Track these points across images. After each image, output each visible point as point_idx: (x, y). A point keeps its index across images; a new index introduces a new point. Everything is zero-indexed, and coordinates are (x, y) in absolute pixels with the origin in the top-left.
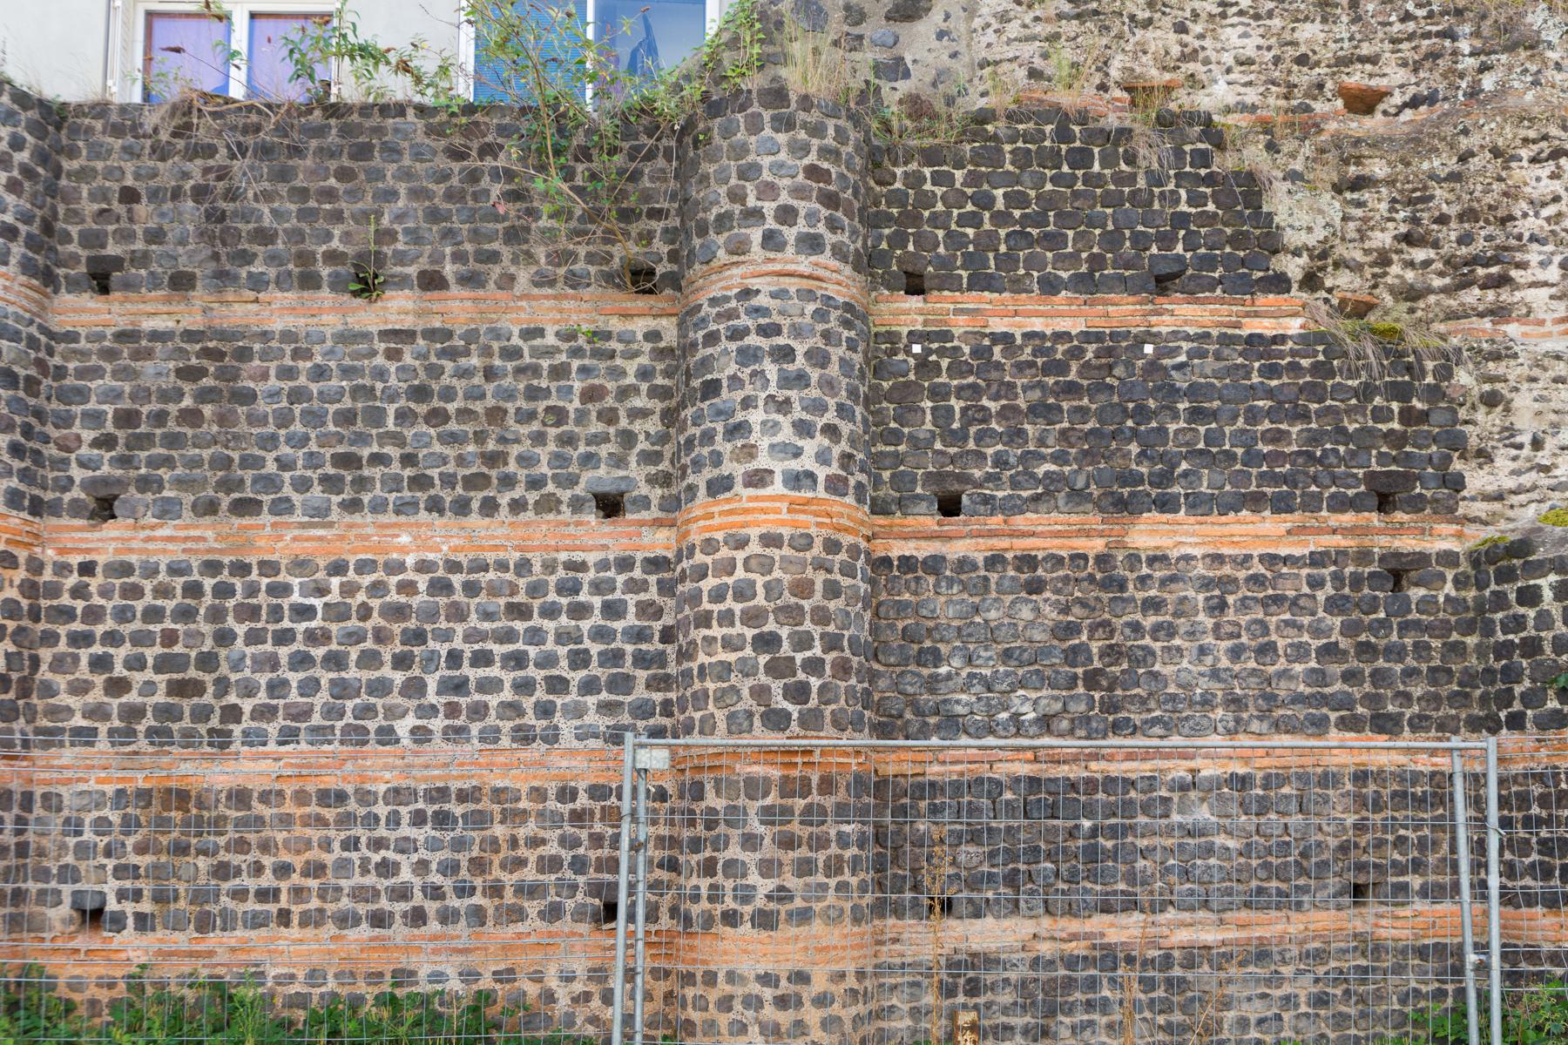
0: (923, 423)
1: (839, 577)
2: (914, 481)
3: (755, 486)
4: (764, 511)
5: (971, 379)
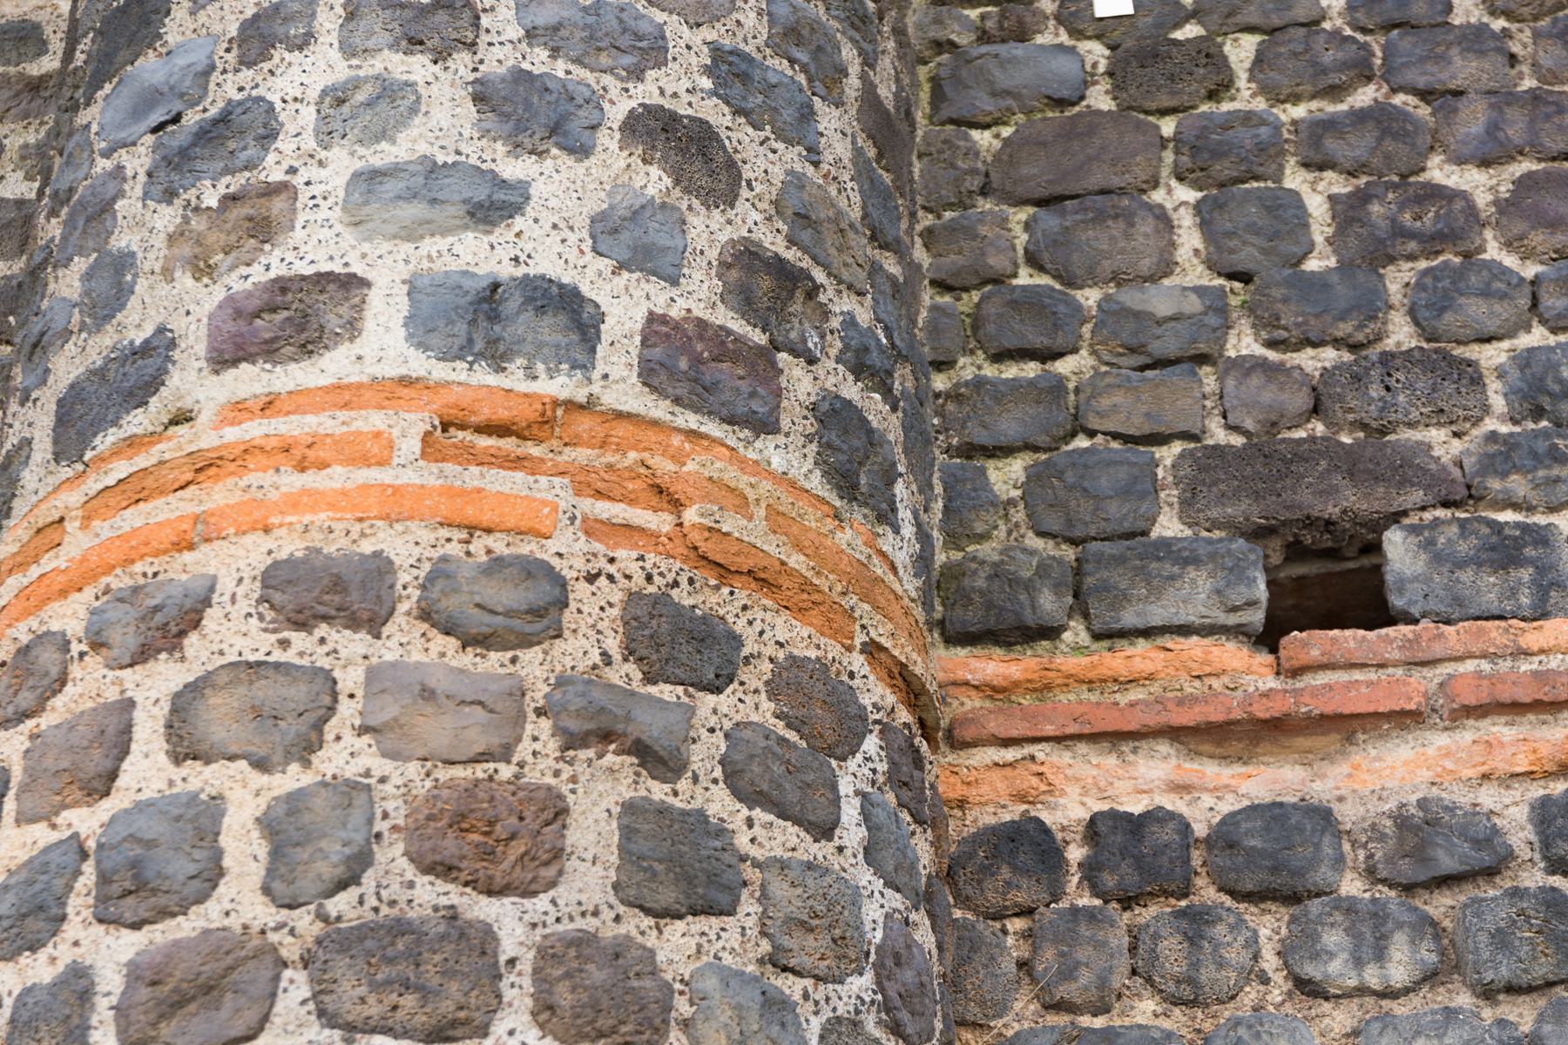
0: (1167, 267)
1: (720, 803)
2: (1144, 487)
3: (269, 351)
4: (302, 455)
5: (1365, 96)
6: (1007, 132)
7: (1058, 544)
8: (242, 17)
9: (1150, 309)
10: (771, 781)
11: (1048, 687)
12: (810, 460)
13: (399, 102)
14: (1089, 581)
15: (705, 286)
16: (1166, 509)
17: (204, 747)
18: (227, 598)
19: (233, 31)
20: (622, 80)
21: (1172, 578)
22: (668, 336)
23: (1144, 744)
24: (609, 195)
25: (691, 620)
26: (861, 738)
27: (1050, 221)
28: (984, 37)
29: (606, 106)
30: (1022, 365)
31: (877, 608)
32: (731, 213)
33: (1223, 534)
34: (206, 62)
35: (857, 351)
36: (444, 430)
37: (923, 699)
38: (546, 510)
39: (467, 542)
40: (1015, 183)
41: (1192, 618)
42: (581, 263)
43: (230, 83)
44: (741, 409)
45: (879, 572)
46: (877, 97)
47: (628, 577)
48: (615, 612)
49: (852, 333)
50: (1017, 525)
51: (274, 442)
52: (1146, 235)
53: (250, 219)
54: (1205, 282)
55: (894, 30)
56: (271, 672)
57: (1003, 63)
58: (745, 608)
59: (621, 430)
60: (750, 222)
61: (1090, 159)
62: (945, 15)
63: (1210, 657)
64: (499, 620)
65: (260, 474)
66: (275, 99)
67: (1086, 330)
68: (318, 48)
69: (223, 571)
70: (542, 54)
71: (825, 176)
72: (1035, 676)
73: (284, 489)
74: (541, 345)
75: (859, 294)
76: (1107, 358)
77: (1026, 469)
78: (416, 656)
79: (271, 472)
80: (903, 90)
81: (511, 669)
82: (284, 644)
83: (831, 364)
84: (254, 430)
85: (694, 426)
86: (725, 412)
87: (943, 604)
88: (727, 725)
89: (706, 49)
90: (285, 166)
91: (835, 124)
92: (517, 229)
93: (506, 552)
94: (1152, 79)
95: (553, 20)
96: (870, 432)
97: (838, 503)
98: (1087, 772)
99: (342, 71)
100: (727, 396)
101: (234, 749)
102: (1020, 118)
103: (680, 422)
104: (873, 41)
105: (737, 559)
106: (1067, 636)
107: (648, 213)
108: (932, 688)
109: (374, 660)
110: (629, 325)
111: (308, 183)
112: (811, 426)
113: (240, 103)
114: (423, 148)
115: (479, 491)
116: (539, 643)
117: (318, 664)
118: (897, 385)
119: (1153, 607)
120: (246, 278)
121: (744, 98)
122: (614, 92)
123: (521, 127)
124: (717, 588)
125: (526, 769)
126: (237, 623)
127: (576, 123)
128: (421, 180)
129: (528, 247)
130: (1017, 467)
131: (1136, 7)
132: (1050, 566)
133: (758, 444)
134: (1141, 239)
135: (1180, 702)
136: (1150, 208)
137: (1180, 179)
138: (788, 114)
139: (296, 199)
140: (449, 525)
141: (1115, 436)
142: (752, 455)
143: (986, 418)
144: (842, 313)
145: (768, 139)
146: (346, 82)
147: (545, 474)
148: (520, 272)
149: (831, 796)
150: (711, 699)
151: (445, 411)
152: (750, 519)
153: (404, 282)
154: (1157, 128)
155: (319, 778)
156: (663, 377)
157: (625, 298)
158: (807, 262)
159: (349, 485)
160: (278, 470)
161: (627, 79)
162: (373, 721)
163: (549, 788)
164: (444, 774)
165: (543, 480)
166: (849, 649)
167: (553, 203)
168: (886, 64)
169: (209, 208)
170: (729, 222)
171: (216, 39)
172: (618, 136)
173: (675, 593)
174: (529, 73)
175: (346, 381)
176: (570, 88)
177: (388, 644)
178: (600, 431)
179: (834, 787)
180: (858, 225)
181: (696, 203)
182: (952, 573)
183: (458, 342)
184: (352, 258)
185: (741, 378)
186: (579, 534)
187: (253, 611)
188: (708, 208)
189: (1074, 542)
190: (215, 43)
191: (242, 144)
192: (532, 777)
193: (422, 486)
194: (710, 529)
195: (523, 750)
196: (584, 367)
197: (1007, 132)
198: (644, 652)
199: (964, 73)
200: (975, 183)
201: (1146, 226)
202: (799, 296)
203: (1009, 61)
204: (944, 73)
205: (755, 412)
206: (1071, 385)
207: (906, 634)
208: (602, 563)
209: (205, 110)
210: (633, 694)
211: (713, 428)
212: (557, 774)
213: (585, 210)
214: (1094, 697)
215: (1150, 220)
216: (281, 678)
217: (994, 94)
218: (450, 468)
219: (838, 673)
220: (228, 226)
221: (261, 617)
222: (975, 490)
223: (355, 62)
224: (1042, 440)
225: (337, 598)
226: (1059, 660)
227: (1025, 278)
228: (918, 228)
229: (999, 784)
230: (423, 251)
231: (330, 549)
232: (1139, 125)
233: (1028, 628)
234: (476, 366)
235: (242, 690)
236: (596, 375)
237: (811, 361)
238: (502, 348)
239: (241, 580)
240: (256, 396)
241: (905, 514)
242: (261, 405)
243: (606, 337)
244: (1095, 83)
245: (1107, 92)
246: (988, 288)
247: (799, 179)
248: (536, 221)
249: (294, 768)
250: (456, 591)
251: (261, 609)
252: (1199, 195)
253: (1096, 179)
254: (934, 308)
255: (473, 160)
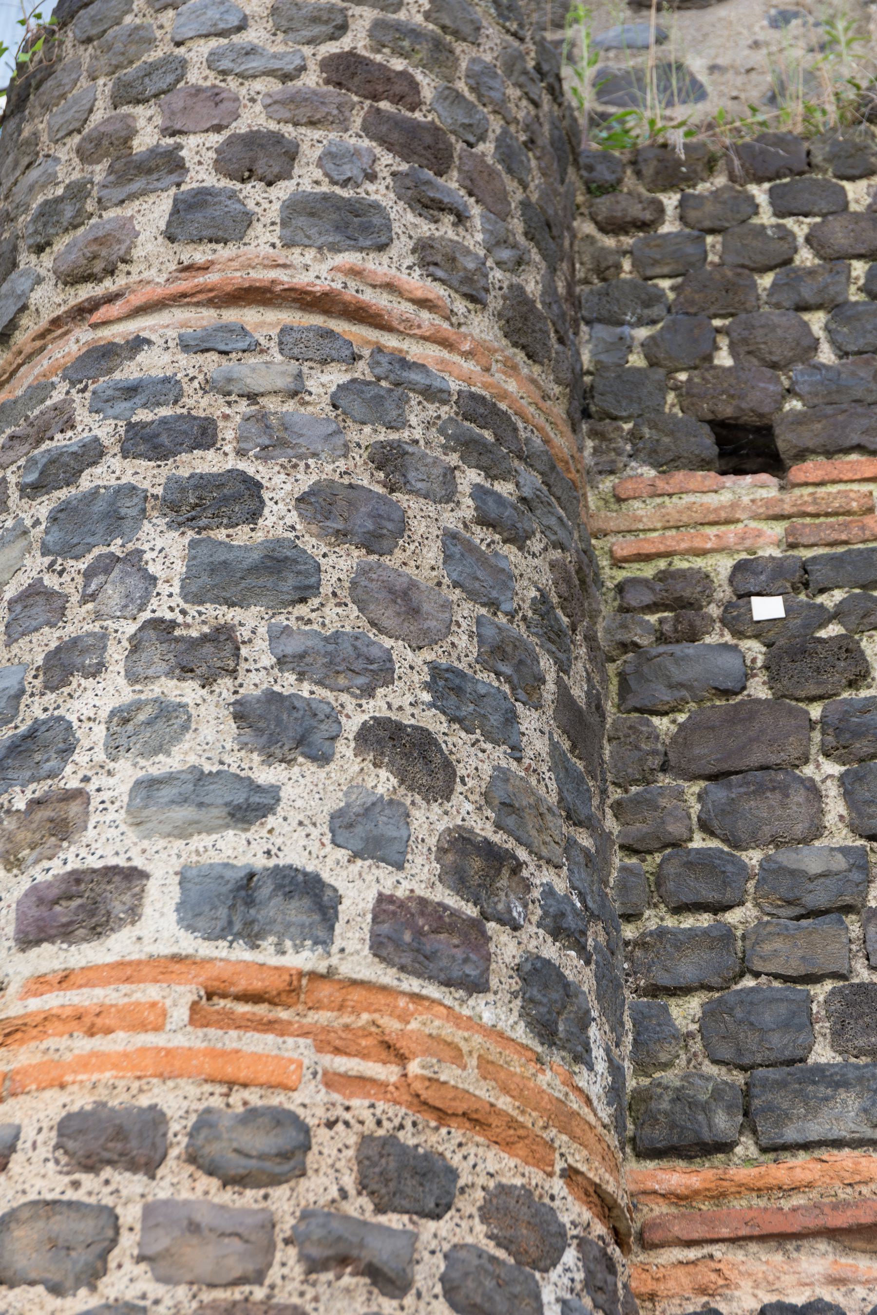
0: (817, 830)
6: (682, 718)
7: (730, 1070)
8: (47, 649)
9: (803, 868)
10: (483, 1295)
11: (723, 1195)
12: (516, 1013)
13: (173, 721)
14: (756, 1103)
15: (426, 869)
16: (820, 1039)
17: (9, 1274)
18: (29, 1144)
19: (40, 660)
20: (356, 697)
21: (826, 1099)
22: (394, 913)
23: (805, 1243)
24: (346, 794)
25: (415, 1157)
26: (561, 1252)
27: (719, 793)
28: (662, 638)
29: (343, 720)
30: (698, 916)
31: (573, 1138)
32: (447, 806)
33: (869, 1060)
34: (17, 687)
35: (555, 917)
36: (209, 998)
37: (616, 1212)
38: (293, 1067)
39: (227, 1095)
40: (689, 761)
41: (844, 1133)
42: (322, 853)
43: (36, 705)
44: (456, 973)
45: (575, 1106)
46: (571, 697)
47: (362, 1123)
48: (351, 1153)
49: (551, 901)
50: (695, 1055)
51: (68, 1012)
52: (799, 805)
53: (52, 821)
54: (849, 843)
55: (586, 638)
56: (64, 1209)
57: (678, 660)
58: (460, 1145)
59: (356, 995)
60: (463, 812)
61: (751, 740)
62: (629, 621)
63: (860, 1167)
64: (253, 1163)
65: (57, 1039)
66: (72, 718)
67: (751, 885)
68: (107, 676)
69: (26, 1122)
70: (291, 678)
71: (527, 769)
72: (713, 1185)
73: (76, 1052)
74: (289, 925)
75: (556, 867)
76: (769, 909)
77: (702, 1006)
78: (185, 1195)
79: (66, 1037)
80: (594, 687)
81: (263, 1205)
82: (76, 1185)
83: (533, 929)
84: (53, 1001)
85: (416, 990)
86: (442, 976)
87: (635, 1124)
88: (446, 1247)
89: (426, 669)
90: (80, 775)
91: (535, 725)
92: (269, 827)
93: (259, 1103)
94: (801, 671)
95: (300, 649)
96: (566, 985)
97: (539, 1049)
98: (758, 1268)
99: (127, 695)
100: (444, 963)
101: (33, 1275)
102: (693, 706)
103: (405, 986)
104: (568, 651)
105: (454, 1104)
106: (739, 1150)
107: (378, 809)
108: (623, 1201)
109: (150, 1198)
110: (362, 905)
111: (99, 790)
112: (515, 984)
113: (44, 722)
114: (193, 760)
115: (237, 1051)
116: (287, 1181)
117: (104, 1202)
118: (590, 942)
119: (811, 1124)
120: (48, 870)
121: (458, 708)
122: (350, 708)
123: (273, 740)
124: (437, 1129)
125: (276, 1291)
126: (37, 1167)
127: (319, 735)
128: (190, 787)
129: (279, 841)
130: (694, 1004)
131: (786, 611)
132: (723, 1090)
133: (471, 1002)
134: (795, 808)
135: (835, 1207)
136: (802, 781)
137: (827, 755)
138: (495, 720)
139: (89, 804)
140: (213, 1081)
141: (776, 976)
142: (466, 1012)
143: (668, 963)
144: (542, 884)
145: (478, 741)
146: (130, 705)
147: (292, 1035)
148: (271, 863)
149: (535, 1305)
150: (431, 1226)
151: (209, 983)
152: (464, 1068)
153: (176, 874)
154: (808, 713)
155: (103, 1301)
156: (391, 949)
157: (358, 883)
158: (511, 844)
159: (130, 1048)
160: (71, 1036)
161: (360, 697)
162: (150, 1251)
163: (295, 1307)
164: (207, 1296)
165: (290, 1041)
166: (550, 1175)
167: (299, 803)
168: (579, 668)
169: (18, 811)
170: (446, 813)
171: (26, 667)
172: (353, 744)
173: (401, 1135)
174: (280, 694)
175: (128, 958)
176: (314, 706)
177: (162, 1184)
178: (338, 996)
179: (537, 1297)
180: (555, 809)
181: (418, 798)
182: (641, 1097)
183: (221, 924)
184: (134, 853)
185: (456, 946)
186: (321, 1087)
187: (50, 1156)
188: (428, 802)
189: (744, 1069)
190: (25, 671)
191: (46, 757)
192: (281, 1298)
193: (190, 1049)
194: (430, 1079)
195: (274, 1274)
196: (324, 943)
197: (682, 718)
198: (374, 1186)
199: (645, 669)
200: (655, 762)
201: (798, 796)
202: (506, 873)
203: (683, 659)
204: (629, 669)
205: (468, 976)
206: (739, 933)
207: (599, 1158)
208: (339, 1112)
209: (16, 727)
210: (365, 1223)
211: (433, 991)
212: (302, 1294)
213: (325, 809)
214: (762, 1203)
215: (802, 791)
216: (73, 1214)
217: (670, 687)
218: (212, 1032)
219: (541, 1197)
220: (34, 826)
221: (57, 1162)
222: (659, 1025)
223: (138, 687)
224: (716, 981)
225: (119, 1146)
226: (732, 1171)
227: (698, 842)
228: (609, 802)
229: (682, 1280)
230: (192, 848)
231: (114, 1103)
232: (791, 711)
233: (707, 1144)
234: (235, 945)
235: (41, 1224)
236: (335, 949)
237: (516, 928)
238: (256, 928)
239: (40, 1130)
240: (54, 971)
241: (598, 1052)
242: (58, 979)
243: (342, 917)
244: (755, 675)
245: (764, 683)
246: (669, 850)
247: (504, 773)
248: (285, 819)
249: (83, 1292)
250: (218, 1138)
251: (57, 1154)
252: (843, 769)
253: (756, 757)
254: (624, 869)
255: (234, 769)
